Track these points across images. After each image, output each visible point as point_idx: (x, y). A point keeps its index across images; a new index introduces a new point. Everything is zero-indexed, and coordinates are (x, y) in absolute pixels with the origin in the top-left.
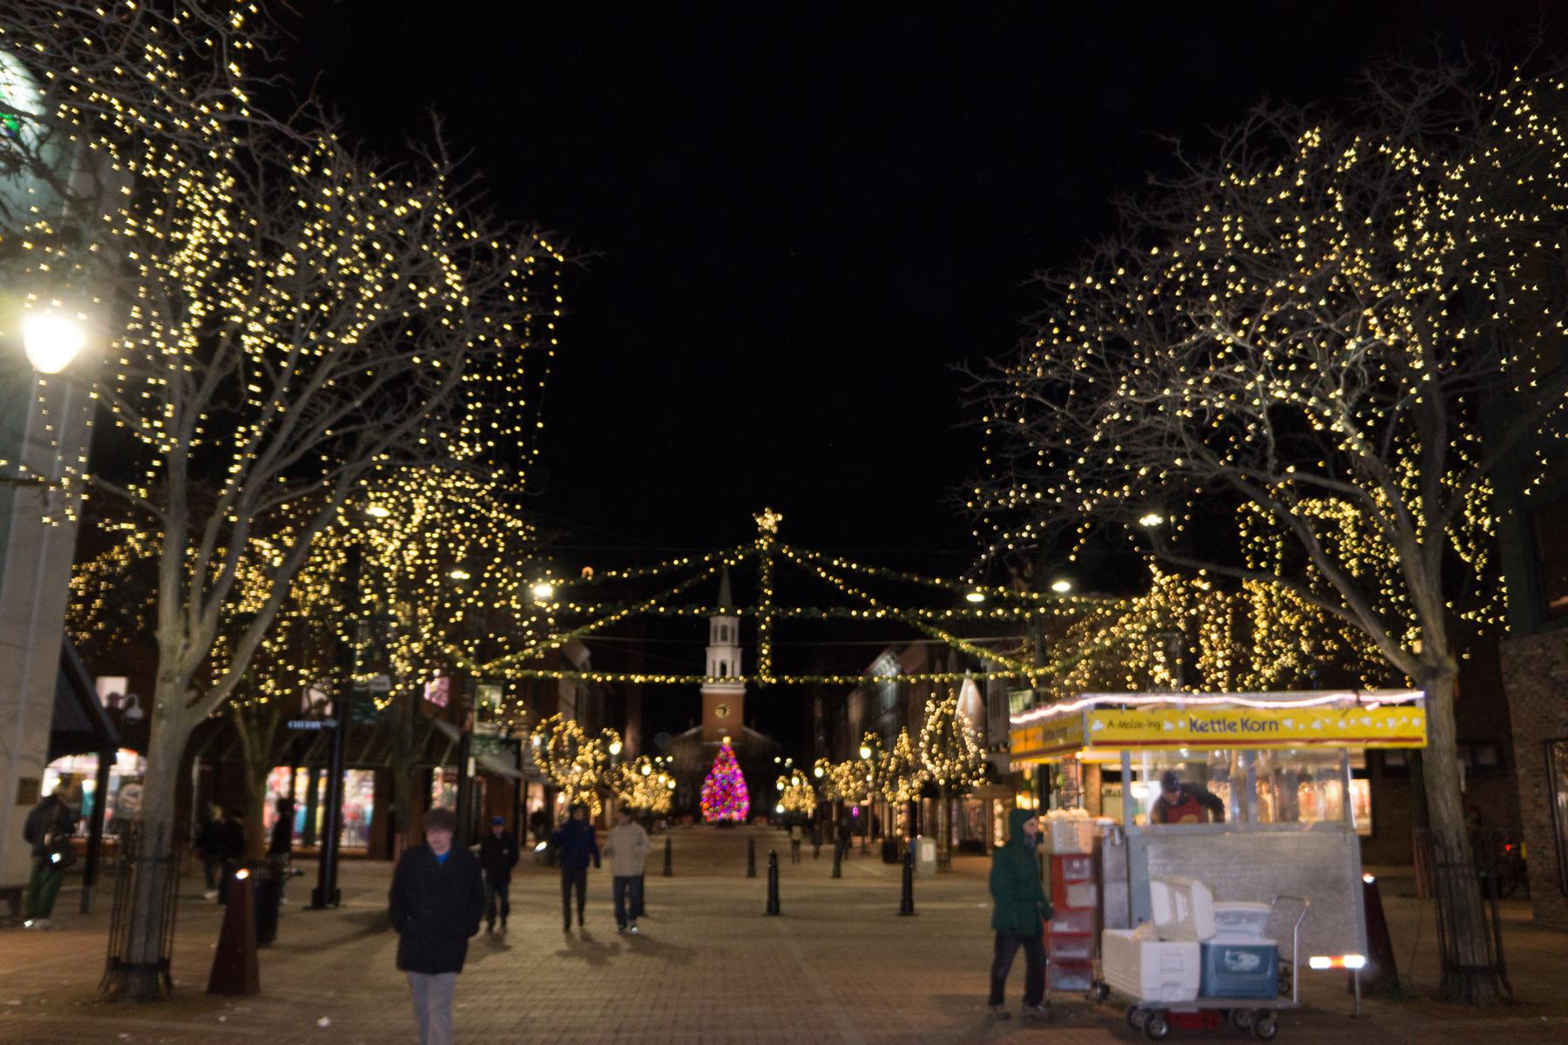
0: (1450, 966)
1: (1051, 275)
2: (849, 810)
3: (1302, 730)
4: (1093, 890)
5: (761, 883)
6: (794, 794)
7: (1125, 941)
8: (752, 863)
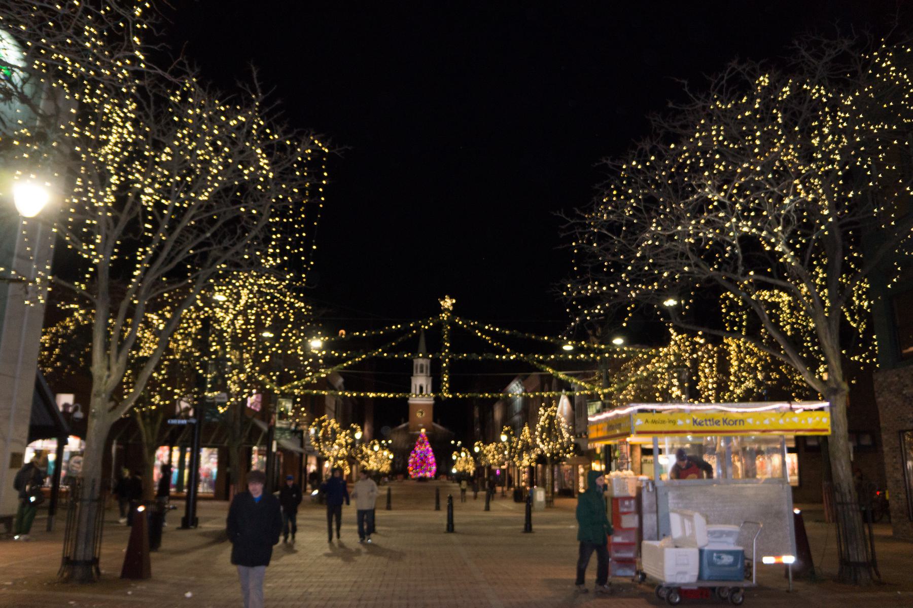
0: (845, 562)
1: (612, 160)
2: (494, 471)
3: (758, 425)
4: (636, 518)
5: (443, 514)
6: (462, 462)
7: (655, 548)
8: (438, 502)
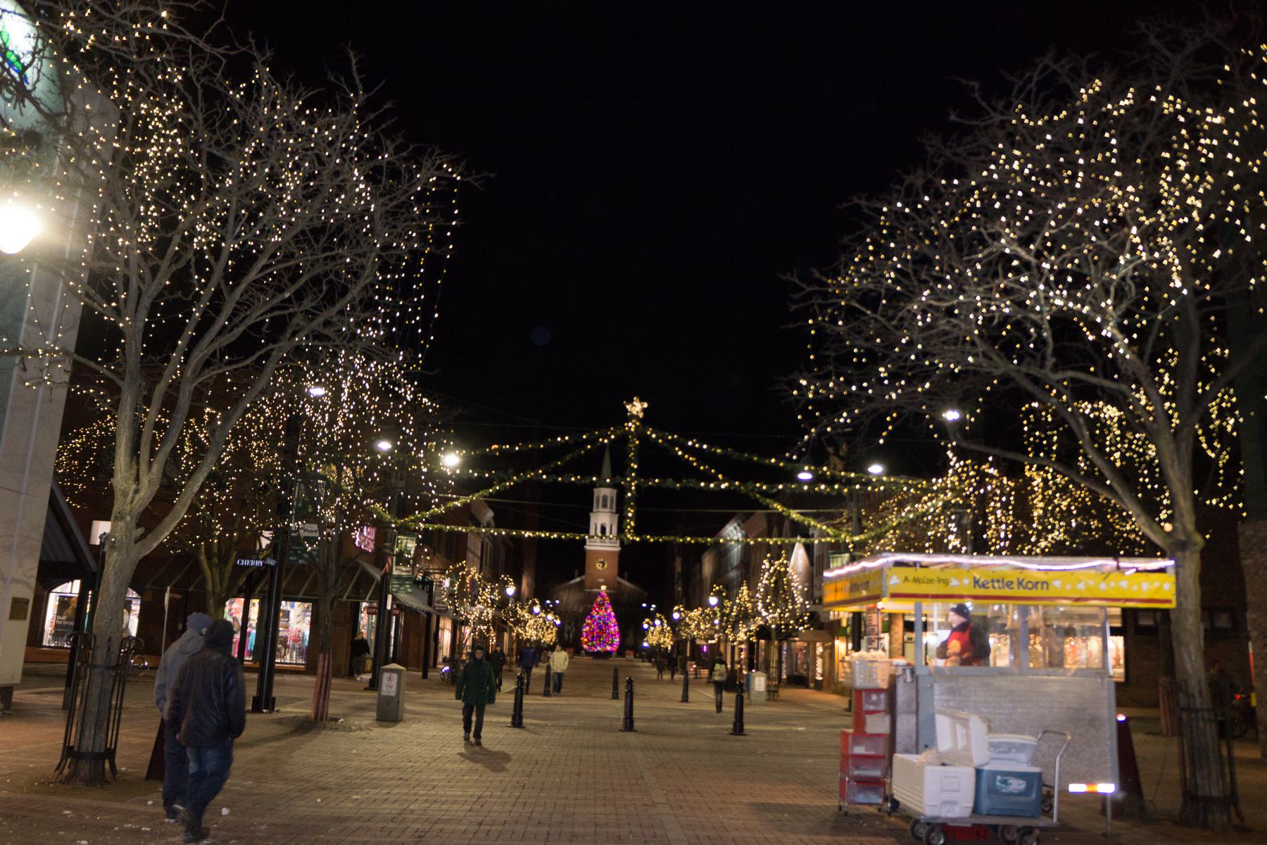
0: (1190, 795)
1: (868, 199)
2: (700, 647)
3: (1069, 590)
4: (887, 719)
5: (620, 704)
6: (657, 634)
7: (912, 765)
8: (616, 687)
